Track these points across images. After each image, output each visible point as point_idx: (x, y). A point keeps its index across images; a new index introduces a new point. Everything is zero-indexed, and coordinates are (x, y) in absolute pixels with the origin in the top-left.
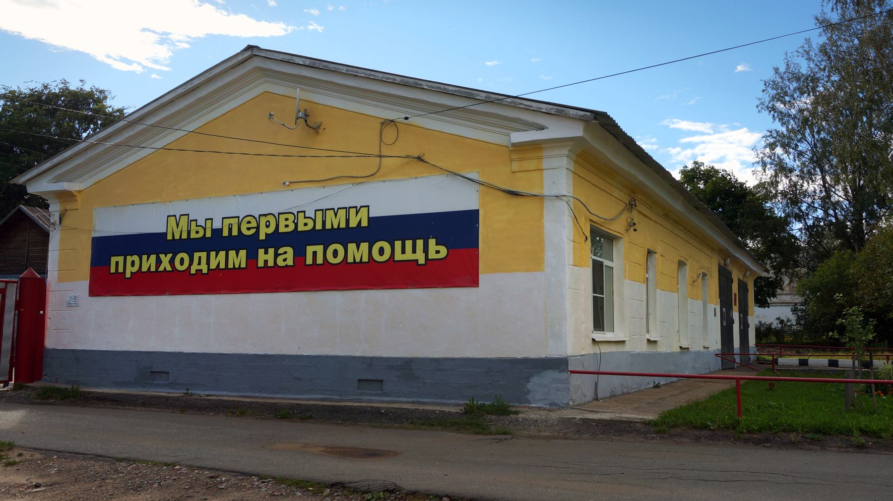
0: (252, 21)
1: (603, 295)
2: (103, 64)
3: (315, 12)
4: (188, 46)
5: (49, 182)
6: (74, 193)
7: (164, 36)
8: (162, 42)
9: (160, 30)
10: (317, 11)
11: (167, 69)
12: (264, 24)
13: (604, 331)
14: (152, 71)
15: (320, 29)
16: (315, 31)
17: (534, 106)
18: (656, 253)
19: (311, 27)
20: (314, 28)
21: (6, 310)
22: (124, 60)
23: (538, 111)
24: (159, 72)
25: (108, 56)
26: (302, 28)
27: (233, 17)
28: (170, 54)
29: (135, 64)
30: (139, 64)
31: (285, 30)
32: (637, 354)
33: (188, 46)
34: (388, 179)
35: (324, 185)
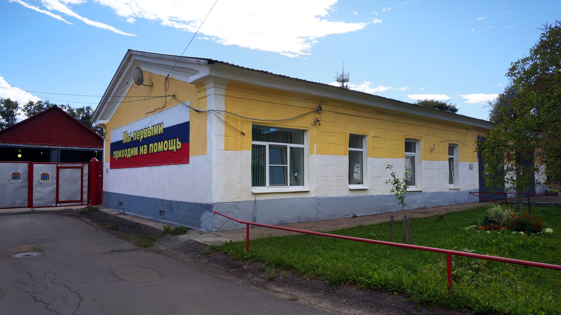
0: (346, 24)
1: (287, 165)
2: (283, 55)
3: (376, 14)
4: (317, 42)
5: (99, 120)
6: (106, 125)
7: (308, 39)
8: (306, 42)
9: (305, 36)
10: (377, 13)
11: (309, 54)
12: (352, 25)
13: (287, 186)
14: (304, 56)
15: (380, 21)
16: (378, 23)
17: (194, 61)
18: (367, 136)
19: (375, 22)
20: (377, 21)
21: (84, 175)
22: (291, 53)
23: (192, 63)
24: (306, 56)
25: (284, 52)
26: (371, 22)
27: (338, 23)
28: (310, 47)
29: (296, 54)
30: (298, 54)
31: (363, 25)
32: (348, 197)
33: (317, 42)
34: (168, 108)
35: (153, 113)
